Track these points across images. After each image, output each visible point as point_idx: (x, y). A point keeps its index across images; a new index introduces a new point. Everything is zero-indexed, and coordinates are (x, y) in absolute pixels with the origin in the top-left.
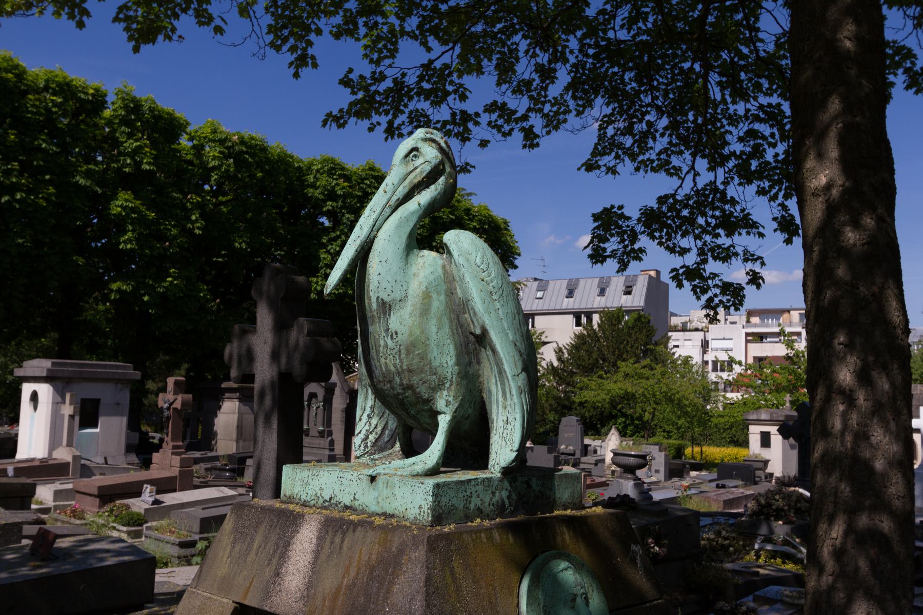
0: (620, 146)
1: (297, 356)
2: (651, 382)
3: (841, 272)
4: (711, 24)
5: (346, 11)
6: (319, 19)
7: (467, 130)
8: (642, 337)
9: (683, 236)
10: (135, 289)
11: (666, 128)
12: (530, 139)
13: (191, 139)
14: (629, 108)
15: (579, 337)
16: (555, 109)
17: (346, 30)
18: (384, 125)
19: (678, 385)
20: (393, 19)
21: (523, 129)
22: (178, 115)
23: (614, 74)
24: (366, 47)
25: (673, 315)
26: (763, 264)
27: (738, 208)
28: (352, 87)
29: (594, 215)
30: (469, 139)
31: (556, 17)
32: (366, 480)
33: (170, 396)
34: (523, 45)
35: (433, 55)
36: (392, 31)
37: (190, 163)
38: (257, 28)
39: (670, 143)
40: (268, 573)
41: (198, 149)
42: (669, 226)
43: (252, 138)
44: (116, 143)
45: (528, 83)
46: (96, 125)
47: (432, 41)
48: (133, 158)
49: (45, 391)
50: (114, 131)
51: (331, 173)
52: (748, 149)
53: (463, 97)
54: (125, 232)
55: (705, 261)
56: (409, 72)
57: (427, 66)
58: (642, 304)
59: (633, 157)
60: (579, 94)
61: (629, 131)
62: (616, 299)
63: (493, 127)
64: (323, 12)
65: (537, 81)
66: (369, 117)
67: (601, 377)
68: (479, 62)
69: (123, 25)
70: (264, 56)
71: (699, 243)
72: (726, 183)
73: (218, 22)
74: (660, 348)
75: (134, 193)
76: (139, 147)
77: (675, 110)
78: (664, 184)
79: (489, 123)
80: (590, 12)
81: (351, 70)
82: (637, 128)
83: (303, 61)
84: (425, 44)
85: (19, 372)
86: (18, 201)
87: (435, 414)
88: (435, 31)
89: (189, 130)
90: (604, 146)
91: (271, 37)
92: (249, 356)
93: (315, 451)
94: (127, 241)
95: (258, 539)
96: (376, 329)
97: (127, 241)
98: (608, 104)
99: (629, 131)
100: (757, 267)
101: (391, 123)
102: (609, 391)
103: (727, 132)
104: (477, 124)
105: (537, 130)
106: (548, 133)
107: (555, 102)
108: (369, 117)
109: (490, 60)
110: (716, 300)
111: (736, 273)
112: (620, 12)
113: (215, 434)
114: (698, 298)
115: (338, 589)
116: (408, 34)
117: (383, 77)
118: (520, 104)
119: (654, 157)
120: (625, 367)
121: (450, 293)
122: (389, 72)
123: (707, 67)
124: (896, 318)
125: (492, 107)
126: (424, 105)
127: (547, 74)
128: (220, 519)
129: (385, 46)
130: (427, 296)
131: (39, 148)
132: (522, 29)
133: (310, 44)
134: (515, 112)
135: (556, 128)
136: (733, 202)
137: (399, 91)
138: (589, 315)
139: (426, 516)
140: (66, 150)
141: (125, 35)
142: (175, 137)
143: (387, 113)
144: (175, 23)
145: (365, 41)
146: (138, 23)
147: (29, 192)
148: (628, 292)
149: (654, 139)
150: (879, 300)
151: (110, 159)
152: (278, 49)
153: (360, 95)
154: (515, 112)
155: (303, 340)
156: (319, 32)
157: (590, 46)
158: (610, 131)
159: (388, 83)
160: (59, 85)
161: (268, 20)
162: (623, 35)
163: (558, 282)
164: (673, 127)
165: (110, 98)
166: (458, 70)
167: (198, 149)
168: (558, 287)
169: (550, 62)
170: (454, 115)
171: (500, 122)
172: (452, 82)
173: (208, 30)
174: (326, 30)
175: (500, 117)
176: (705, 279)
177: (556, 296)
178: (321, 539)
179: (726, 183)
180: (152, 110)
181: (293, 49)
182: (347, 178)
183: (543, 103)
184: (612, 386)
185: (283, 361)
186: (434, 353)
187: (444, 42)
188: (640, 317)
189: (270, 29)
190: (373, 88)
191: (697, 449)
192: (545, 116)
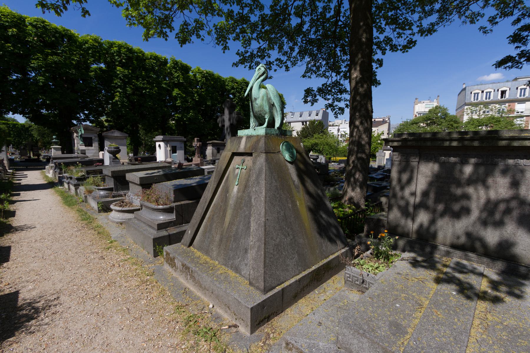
0: (312, 70)
1: (234, 120)
2: (323, 139)
3: (358, 98)
4: (338, 32)
5: (236, 32)
6: (229, 35)
7: (271, 67)
8: (321, 128)
9: (328, 95)
10: (182, 117)
11: (325, 64)
12: (287, 68)
13: (193, 72)
14: (315, 59)
15: (303, 128)
16: (294, 59)
17: (237, 38)
18: (248, 66)
19: (330, 140)
20: (249, 35)
21: (285, 66)
22: (188, 65)
23: (311, 48)
24: (242, 43)
25: (330, 122)
27: (343, 87)
28: (239, 55)
30: (271, 69)
31: (294, 31)
33: (196, 143)
34: (286, 41)
35: (261, 45)
36: (249, 38)
37: (193, 80)
38: (213, 39)
39: (326, 69)
40: (237, 147)
41: (195, 76)
42: (325, 93)
43: (210, 72)
44: (172, 74)
45: (287, 52)
46: (165, 69)
47: (260, 41)
48: (177, 79)
49: (162, 144)
50: (171, 71)
51: (232, 81)
52: (347, 70)
53: (269, 57)
54: (177, 100)
55: (334, 102)
56: (255, 50)
57: (259, 48)
59: (315, 73)
60: (301, 55)
61: (315, 65)
62: (314, 117)
64: (230, 33)
65: (289, 51)
66: (244, 64)
67: (308, 139)
68: (273, 46)
69: (177, 39)
70: (215, 47)
71: (333, 97)
72: (340, 80)
73: (202, 37)
74: (325, 131)
75: (179, 89)
76: (179, 75)
77: (327, 60)
78: (323, 80)
79: (276, 64)
80: (304, 30)
81: (239, 50)
82: (317, 64)
83: (226, 48)
84: (258, 42)
85: (154, 139)
86: (148, 92)
87: (265, 119)
88: (261, 38)
89: (192, 69)
90: (308, 70)
91: (216, 41)
92: (223, 121)
94: (178, 103)
95: (235, 142)
96: (254, 103)
97: (178, 103)
98: (309, 58)
99: (315, 65)
101: (250, 65)
103: (341, 65)
104: (273, 65)
105: (289, 66)
106: (293, 67)
107: (294, 57)
108: (244, 64)
109: (276, 45)
110: (337, 112)
112: (312, 30)
113: (206, 155)
116: (254, 39)
117: (247, 52)
118: (284, 58)
119: (321, 73)
120: (316, 136)
121: (267, 96)
122: (249, 50)
123: (336, 46)
124: (370, 108)
125: (277, 60)
126: (259, 60)
127: (292, 49)
128: (213, 172)
129: (247, 43)
130: (263, 97)
131: (151, 76)
132: (285, 36)
133: (227, 43)
134: (283, 61)
135: (295, 65)
136: (342, 85)
137: (252, 56)
138: (306, 122)
139: (264, 134)
140: (158, 77)
141: (178, 42)
142: (188, 72)
143: (249, 63)
144: (191, 38)
145: (242, 41)
146: (181, 38)
147: (150, 89)
148: (317, 115)
149: (322, 68)
150: (366, 104)
151: (170, 79)
152: (219, 44)
153: (242, 57)
154: (283, 61)
155: (236, 116)
156: (229, 39)
157: (304, 40)
158: (310, 66)
159: (249, 54)
160: (154, 57)
161: (215, 36)
162: (313, 37)
164: (327, 64)
165: (169, 61)
166: (268, 49)
167: (195, 76)
168: (297, 114)
169: (293, 46)
170: (267, 62)
171: (279, 64)
172: (266, 53)
173: (200, 40)
174: (231, 38)
175: (279, 62)
176: (334, 107)
177: (297, 117)
178: (246, 139)
179: (340, 80)
180: (181, 64)
181: (222, 45)
182: (237, 83)
183: (291, 58)
184: (312, 141)
185: (231, 121)
186: (265, 107)
187: (264, 41)
188: (320, 122)
189: (217, 39)
190: (245, 55)
191: (334, 158)
192: (291, 62)
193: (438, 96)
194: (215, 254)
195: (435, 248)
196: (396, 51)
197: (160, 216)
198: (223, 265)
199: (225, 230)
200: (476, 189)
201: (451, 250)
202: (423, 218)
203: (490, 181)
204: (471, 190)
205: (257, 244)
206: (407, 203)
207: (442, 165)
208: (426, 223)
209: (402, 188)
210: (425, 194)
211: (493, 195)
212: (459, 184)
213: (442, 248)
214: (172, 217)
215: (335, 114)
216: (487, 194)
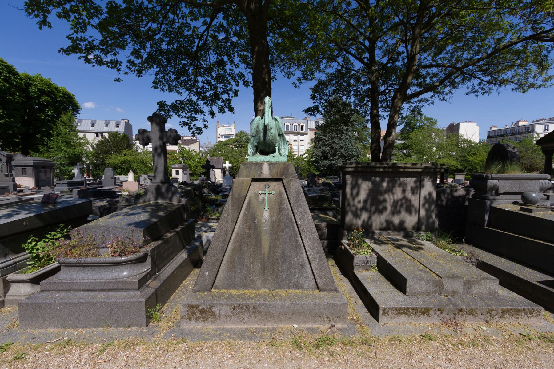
5: (64, 8)
17: (65, 15)
26: (207, 123)
29: (157, 103)
32: (272, 157)
58: (123, 131)
62: (112, 128)
63: (128, 68)
93: (3, 183)
100: (206, 123)
102: (120, 160)
111: (200, 124)
114: (190, 131)
115: (277, 172)
163: (87, 121)
193: (234, 122)
194: (259, 283)
195: (373, 233)
196: (247, 86)
197: (123, 271)
198: (277, 288)
199: (266, 255)
200: (389, 195)
201: (381, 232)
202: (365, 216)
203: (394, 191)
204: (386, 196)
205: (317, 256)
206: (357, 208)
207: (374, 182)
208: (366, 219)
209: (354, 199)
210: (365, 201)
211: (396, 197)
212: (382, 194)
213: (377, 232)
214: (146, 268)
215: (192, 133)
216: (393, 197)
